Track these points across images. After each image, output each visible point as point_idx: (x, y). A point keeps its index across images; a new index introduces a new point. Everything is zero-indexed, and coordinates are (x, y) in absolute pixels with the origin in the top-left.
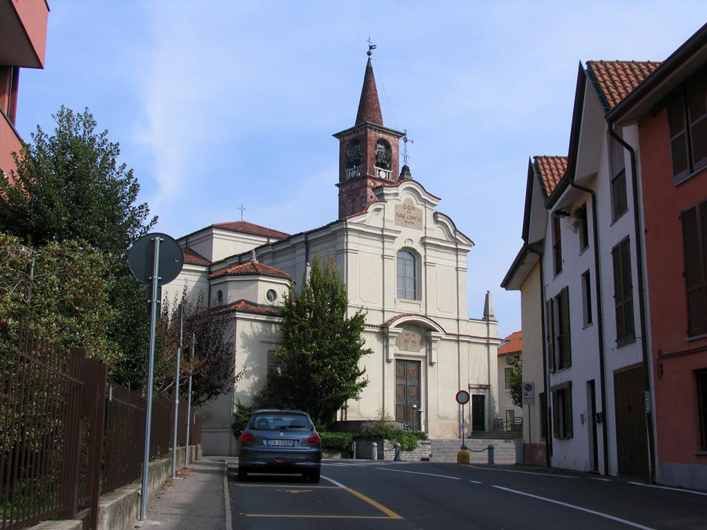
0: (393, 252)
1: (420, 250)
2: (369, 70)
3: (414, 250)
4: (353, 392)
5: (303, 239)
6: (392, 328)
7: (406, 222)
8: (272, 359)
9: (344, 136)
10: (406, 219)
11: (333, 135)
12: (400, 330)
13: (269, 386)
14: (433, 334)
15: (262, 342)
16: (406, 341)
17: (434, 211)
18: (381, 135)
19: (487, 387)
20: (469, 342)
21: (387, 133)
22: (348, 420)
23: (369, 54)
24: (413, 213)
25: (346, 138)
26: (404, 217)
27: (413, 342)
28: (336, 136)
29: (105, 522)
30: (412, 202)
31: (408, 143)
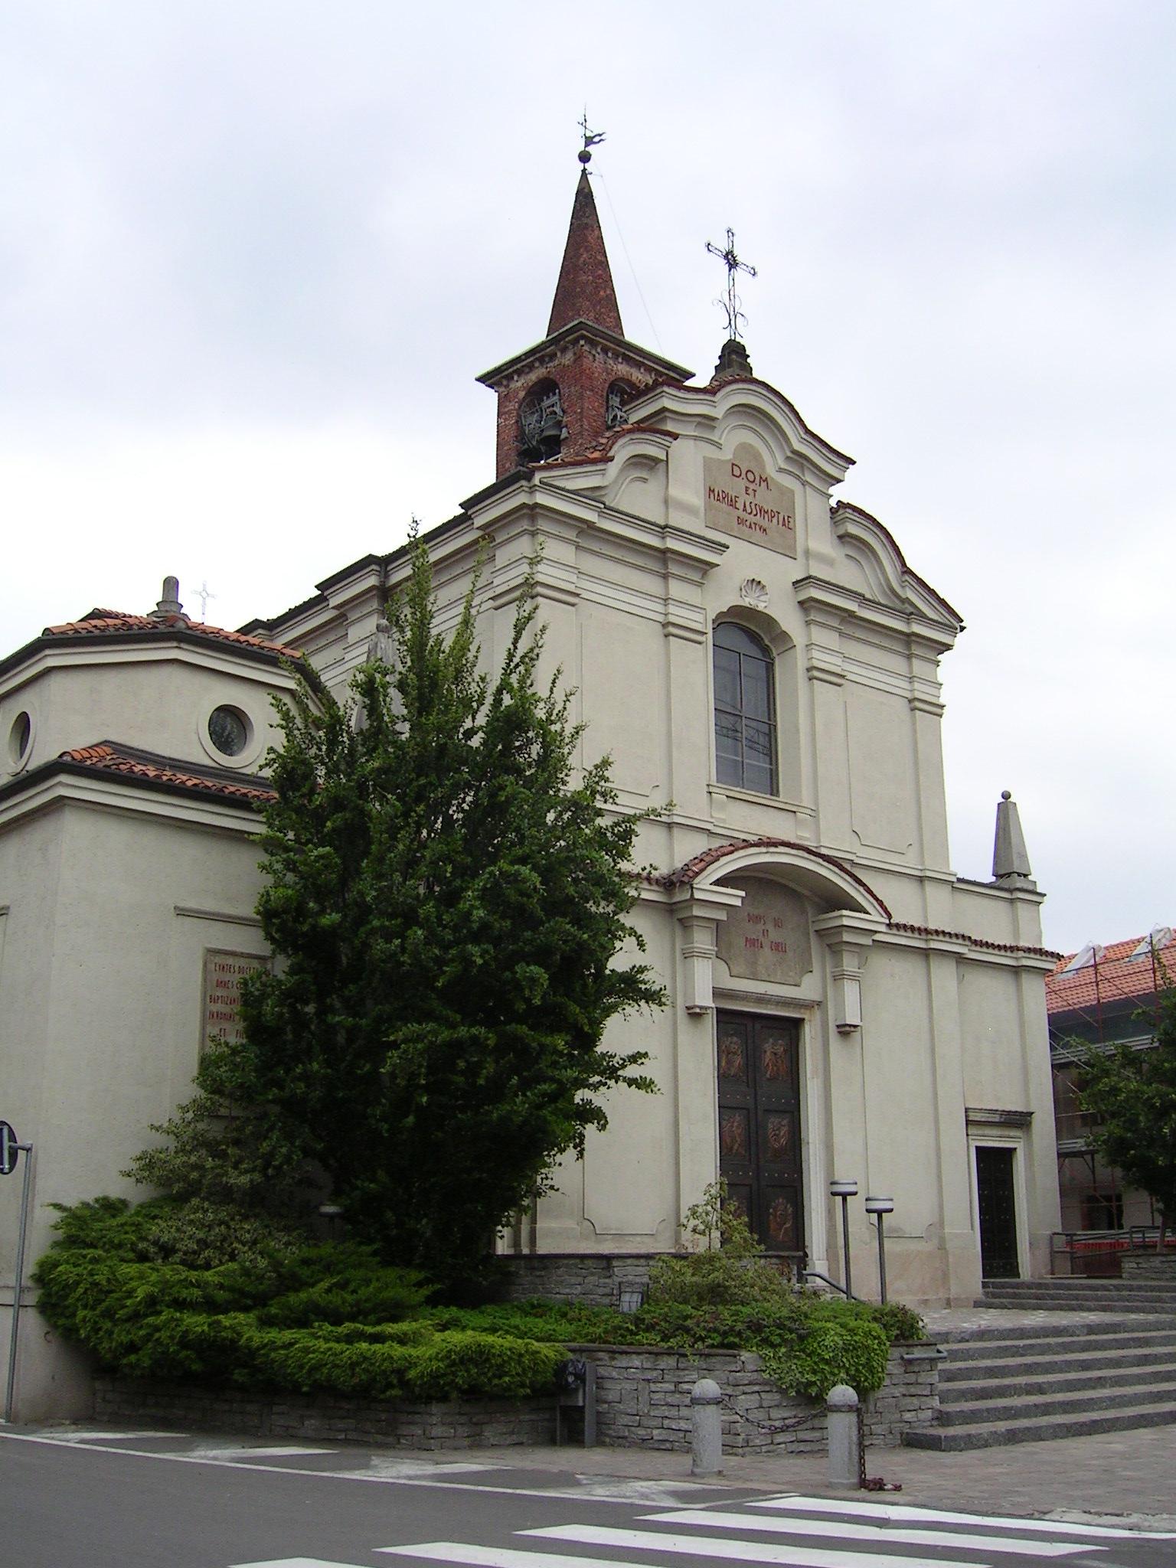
0: (699, 617)
1: (789, 620)
2: (584, 200)
3: (769, 621)
4: (563, 1121)
5: (372, 581)
6: (705, 886)
7: (740, 521)
8: (221, 984)
9: (510, 378)
10: (740, 513)
11: (481, 379)
12: (734, 897)
13: (203, 1111)
14: (849, 918)
15: (182, 912)
16: (752, 943)
17: (833, 503)
18: (622, 369)
19: (1019, 1121)
20: (960, 958)
21: (639, 365)
22: (542, 1249)
23: (585, 157)
24: (765, 498)
25: (519, 384)
26: (732, 503)
27: (778, 947)
28: (488, 379)
29: (457, 1338)
30: (757, 457)
31: (739, 273)
